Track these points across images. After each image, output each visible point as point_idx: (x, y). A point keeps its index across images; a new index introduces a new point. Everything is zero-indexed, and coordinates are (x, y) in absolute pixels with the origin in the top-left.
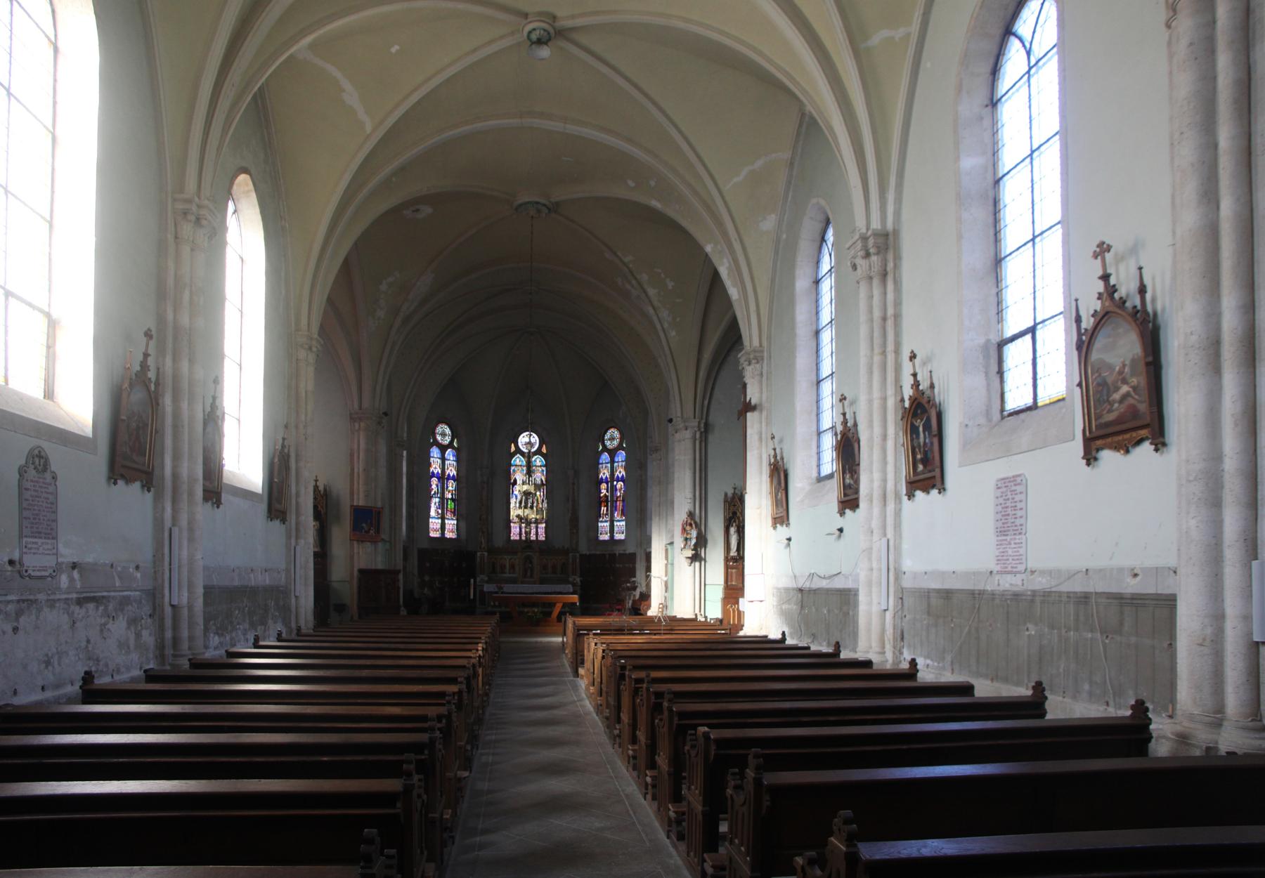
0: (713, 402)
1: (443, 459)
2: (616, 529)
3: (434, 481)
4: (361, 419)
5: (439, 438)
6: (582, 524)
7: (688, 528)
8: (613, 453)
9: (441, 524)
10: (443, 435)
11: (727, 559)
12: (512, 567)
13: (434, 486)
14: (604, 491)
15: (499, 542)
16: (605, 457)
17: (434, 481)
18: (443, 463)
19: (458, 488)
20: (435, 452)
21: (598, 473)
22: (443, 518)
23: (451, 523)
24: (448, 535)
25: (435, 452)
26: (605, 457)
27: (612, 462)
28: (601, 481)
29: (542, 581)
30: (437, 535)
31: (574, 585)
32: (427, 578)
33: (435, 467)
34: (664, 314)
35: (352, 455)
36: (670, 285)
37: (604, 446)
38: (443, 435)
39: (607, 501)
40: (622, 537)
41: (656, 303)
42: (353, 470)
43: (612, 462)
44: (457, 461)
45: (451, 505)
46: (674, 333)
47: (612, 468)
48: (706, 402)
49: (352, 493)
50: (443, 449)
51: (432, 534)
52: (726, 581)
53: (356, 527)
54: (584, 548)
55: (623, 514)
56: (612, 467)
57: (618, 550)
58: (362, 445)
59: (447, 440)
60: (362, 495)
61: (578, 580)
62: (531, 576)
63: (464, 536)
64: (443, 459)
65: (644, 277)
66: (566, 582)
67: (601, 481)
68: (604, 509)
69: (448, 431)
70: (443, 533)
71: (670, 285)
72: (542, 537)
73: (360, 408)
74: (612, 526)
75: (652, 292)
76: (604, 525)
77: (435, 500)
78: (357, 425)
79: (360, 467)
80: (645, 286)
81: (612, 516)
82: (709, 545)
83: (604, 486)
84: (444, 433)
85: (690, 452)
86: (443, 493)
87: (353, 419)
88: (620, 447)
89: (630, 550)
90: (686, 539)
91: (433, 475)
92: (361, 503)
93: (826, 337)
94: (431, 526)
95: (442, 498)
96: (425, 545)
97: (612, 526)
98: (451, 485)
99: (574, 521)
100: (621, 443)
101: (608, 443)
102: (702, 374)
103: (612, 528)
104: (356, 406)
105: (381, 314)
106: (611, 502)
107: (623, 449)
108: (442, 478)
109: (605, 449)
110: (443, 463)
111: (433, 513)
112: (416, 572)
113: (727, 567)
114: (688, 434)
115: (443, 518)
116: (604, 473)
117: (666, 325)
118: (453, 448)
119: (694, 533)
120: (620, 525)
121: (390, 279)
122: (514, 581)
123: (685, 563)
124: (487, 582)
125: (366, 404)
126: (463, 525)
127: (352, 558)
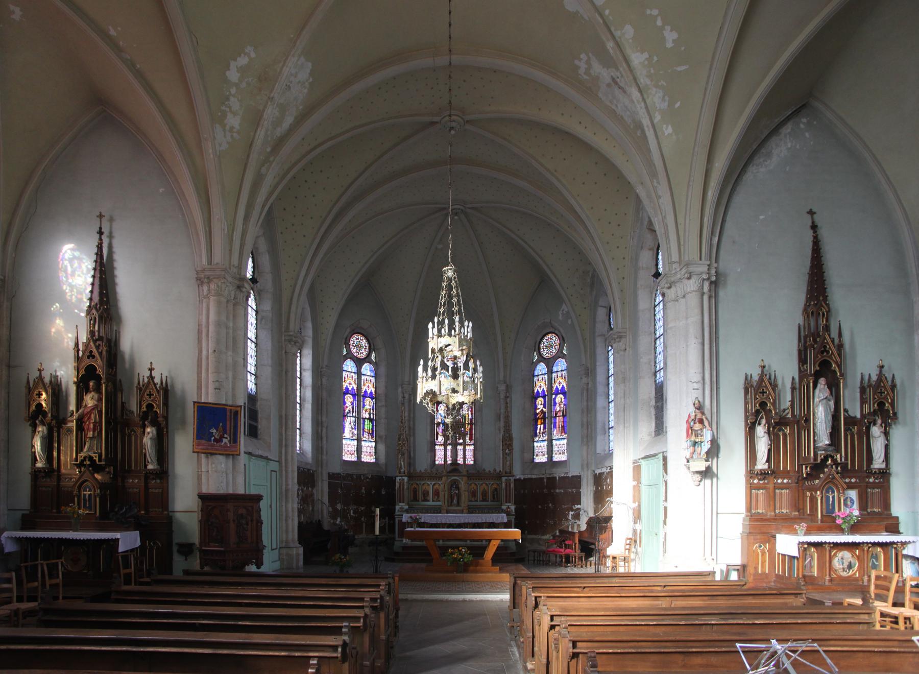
0: (724, 239)
1: (359, 374)
2: (555, 449)
3: (349, 399)
4: (210, 280)
5: (354, 350)
6: (516, 444)
7: (697, 426)
8: (550, 363)
9: (357, 446)
10: (359, 347)
11: (751, 473)
12: (437, 493)
13: (348, 404)
14: (540, 407)
15: (422, 466)
16: (541, 368)
17: (349, 399)
18: (359, 378)
19: (376, 407)
20: (349, 365)
21: (532, 384)
22: (359, 440)
23: (368, 446)
24: (365, 459)
25: (349, 365)
26: (541, 368)
27: (550, 372)
28: (537, 396)
29: (471, 510)
30: (353, 458)
31: (508, 514)
32: (339, 507)
33: (349, 382)
34: (656, 98)
35: (200, 332)
36: (670, 37)
37: (540, 355)
38: (359, 347)
39: (544, 418)
40: (563, 458)
41: (644, 81)
42: (200, 352)
43: (550, 372)
44: (376, 377)
45: (368, 426)
46: (669, 130)
47: (552, 376)
48: (715, 240)
49: (199, 388)
50: (359, 362)
51: (346, 457)
52: (749, 509)
53: (202, 433)
54: (518, 474)
55: (563, 430)
56: (550, 379)
57: (559, 473)
58: (212, 317)
59: (363, 354)
60: (211, 387)
61: (513, 508)
62: (458, 504)
63: (383, 460)
64: (359, 374)
65: (627, 33)
66: (498, 510)
67: (537, 396)
68: (540, 427)
69: (364, 343)
70: (359, 457)
71: (670, 37)
72: (470, 461)
73: (210, 262)
74: (550, 446)
75: (637, 59)
76: (540, 446)
77: (349, 423)
78: (205, 288)
79: (209, 346)
80: (628, 51)
81: (550, 434)
82: (721, 455)
83: (540, 401)
84: (359, 345)
85: (697, 311)
86: (359, 413)
87: (201, 279)
88: (560, 355)
89: (573, 472)
90: (695, 443)
91: (347, 392)
92: (211, 400)
93: (611, 379)
94: (345, 448)
95: (358, 418)
96: (337, 469)
97: (550, 446)
98: (369, 403)
99: (508, 441)
100: (560, 350)
101: (545, 353)
102: (711, 194)
103: (552, 448)
104: (204, 262)
105: (234, 121)
106: (547, 418)
107: (564, 356)
108: (358, 395)
109: (542, 359)
110: (359, 378)
111: (347, 433)
112: (326, 499)
113: (751, 487)
114: (692, 285)
115: (359, 440)
116: (541, 386)
117: (657, 118)
118: (371, 362)
119: (707, 435)
120: (561, 444)
121: (243, 61)
122: (438, 510)
123: (691, 480)
124: (407, 511)
125: (218, 257)
126: (382, 447)
127: (199, 478)
